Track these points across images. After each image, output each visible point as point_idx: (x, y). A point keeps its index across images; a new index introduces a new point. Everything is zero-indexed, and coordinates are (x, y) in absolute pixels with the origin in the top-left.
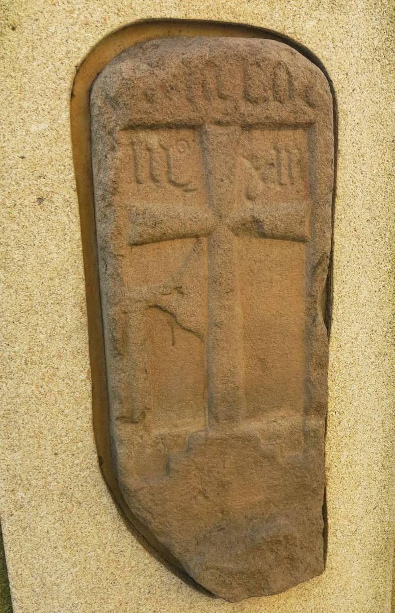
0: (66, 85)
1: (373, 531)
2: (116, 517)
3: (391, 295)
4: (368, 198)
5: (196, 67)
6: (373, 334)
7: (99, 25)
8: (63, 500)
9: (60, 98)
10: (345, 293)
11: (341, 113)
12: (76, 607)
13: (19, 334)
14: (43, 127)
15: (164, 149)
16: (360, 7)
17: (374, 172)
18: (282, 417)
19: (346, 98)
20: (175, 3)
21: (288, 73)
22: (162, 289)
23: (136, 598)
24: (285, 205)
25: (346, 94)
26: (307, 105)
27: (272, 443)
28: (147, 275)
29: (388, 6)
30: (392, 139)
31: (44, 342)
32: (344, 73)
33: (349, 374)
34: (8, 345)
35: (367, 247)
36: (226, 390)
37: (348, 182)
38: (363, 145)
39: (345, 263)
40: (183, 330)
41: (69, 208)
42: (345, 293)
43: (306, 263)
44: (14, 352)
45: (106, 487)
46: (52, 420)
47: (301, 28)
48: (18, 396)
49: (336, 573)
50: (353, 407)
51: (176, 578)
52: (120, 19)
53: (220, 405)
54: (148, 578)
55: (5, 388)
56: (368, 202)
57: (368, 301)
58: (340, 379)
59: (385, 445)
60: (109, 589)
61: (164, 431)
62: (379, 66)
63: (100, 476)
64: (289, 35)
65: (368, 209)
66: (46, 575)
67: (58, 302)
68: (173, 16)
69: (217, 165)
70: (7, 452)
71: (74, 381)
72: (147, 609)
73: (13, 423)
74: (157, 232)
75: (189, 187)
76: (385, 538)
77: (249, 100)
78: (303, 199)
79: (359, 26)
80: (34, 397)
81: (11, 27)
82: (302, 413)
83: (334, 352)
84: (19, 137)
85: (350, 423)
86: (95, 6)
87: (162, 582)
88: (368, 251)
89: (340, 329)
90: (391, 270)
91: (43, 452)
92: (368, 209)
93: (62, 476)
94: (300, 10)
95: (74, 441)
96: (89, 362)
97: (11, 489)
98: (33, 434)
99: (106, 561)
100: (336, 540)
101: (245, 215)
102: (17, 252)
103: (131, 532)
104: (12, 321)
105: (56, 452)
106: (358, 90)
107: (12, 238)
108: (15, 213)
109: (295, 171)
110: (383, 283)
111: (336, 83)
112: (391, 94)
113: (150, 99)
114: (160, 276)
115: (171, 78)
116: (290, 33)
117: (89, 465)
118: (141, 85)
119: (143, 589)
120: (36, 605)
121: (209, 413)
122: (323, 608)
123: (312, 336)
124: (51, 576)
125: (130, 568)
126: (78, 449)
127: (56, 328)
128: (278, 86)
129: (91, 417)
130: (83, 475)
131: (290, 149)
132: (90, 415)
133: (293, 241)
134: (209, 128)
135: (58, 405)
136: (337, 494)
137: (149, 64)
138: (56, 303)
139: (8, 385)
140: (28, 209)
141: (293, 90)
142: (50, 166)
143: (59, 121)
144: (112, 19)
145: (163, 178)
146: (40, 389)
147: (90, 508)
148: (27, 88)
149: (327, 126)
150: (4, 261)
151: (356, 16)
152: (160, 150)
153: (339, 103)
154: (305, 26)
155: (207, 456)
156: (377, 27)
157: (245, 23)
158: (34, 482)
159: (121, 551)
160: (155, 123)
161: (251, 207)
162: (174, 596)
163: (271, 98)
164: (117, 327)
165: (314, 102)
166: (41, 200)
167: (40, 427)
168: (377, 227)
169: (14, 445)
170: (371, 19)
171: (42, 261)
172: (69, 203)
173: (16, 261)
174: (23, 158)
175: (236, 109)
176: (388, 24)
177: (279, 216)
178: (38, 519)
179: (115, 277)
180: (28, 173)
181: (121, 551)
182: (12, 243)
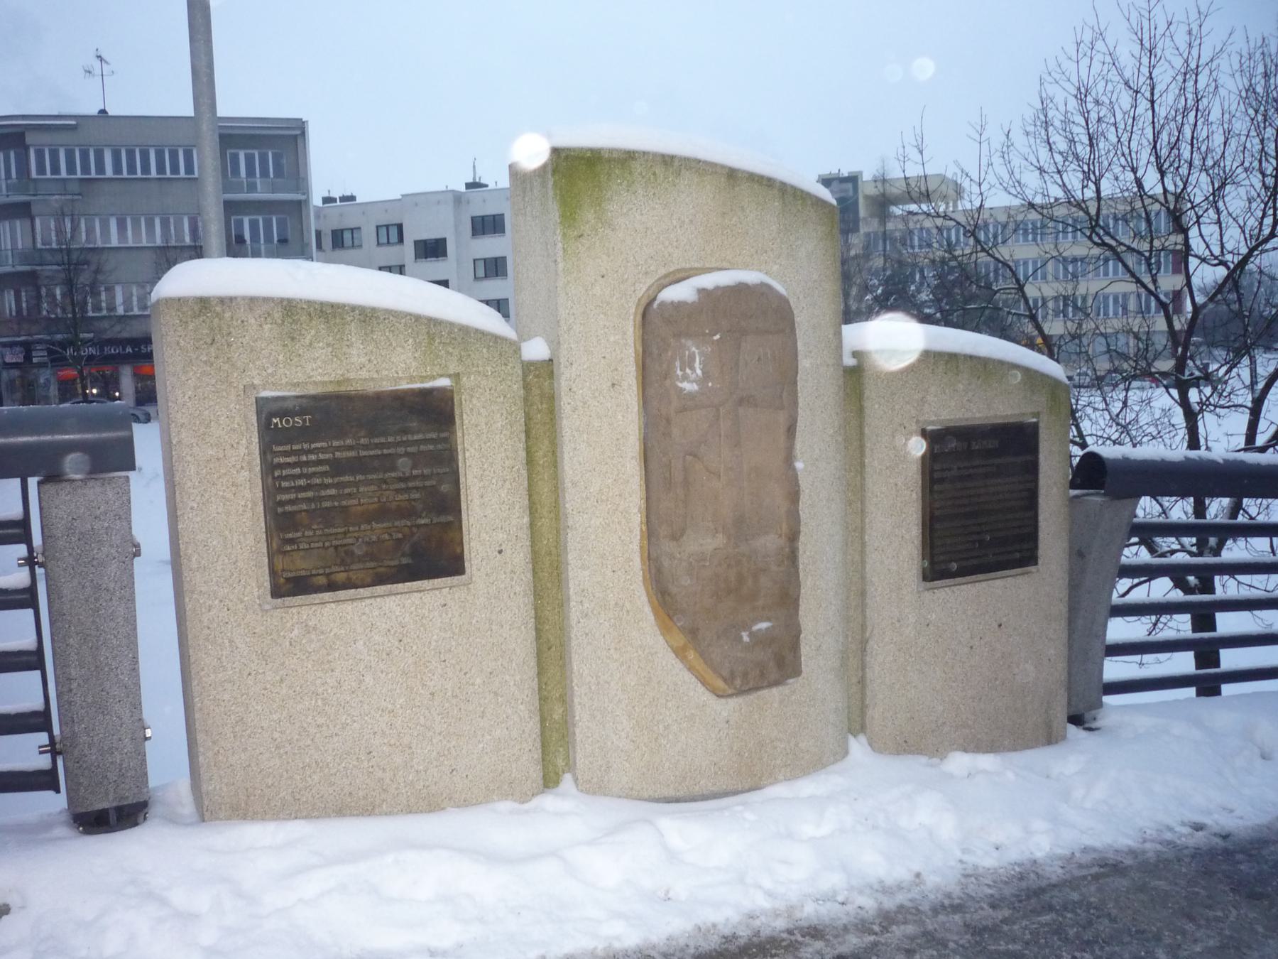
174: (604, 357)
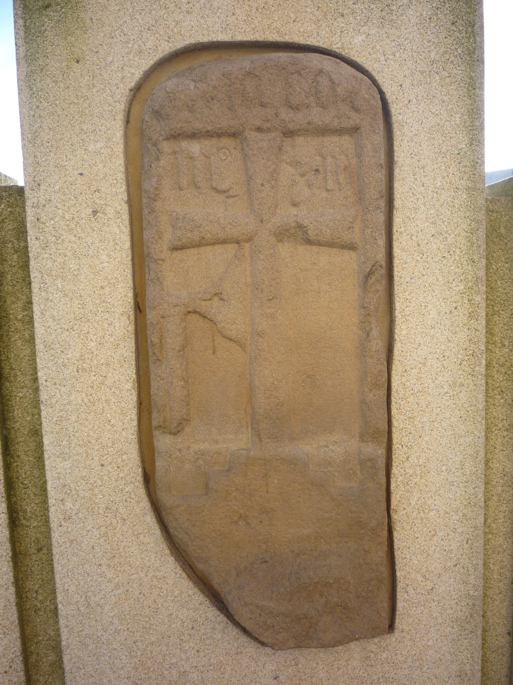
1: (454, 593)
2: (160, 538)
3: (466, 319)
4: (432, 211)
6: (445, 360)
7: (151, 51)
8: (108, 515)
9: (115, 119)
10: (409, 312)
11: (396, 124)
12: (118, 634)
13: (72, 341)
15: (206, 157)
16: (413, 21)
18: (334, 441)
19: (401, 109)
20: (222, 28)
21: (331, 80)
22: (201, 295)
24: (332, 211)
25: (401, 105)
26: (352, 110)
27: (322, 470)
29: (444, 20)
30: (457, 152)
31: (94, 350)
33: (417, 403)
34: (63, 352)
36: (269, 404)
37: (406, 194)
38: (423, 157)
40: (224, 339)
41: (120, 220)
42: (409, 312)
43: (357, 272)
44: (67, 359)
46: (100, 430)
47: (349, 43)
48: (69, 403)
49: (408, 637)
50: (424, 442)
51: (222, 616)
52: (170, 45)
53: (263, 422)
54: (191, 611)
55: (59, 395)
56: (433, 216)
57: (438, 323)
59: (465, 491)
60: (152, 619)
62: (438, 78)
63: (145, 492)
64: (337, 50)
65: (432, 223)
67: (107, 310)
68: (219, 39)
69: (257, 170)
70: (58, 460)
71: (121, 391)
72: (190, 648)
73: (64, 430)
74: (196, 236)
75: (231, 193)
76: (471, 603)
77: (291, 107)
78: (351, 205)
79: (413, 39)
80: (84, 405)
81: (75, 60)
82: (358, 439)
83: (398, 377)
84: (78, 156)
85: (420, 460)
86: (148, 35)
88: (434, 268)
89: (405, 352)
90: (464, 290)
91: (91, 463)
92: (432, 223)
93: (108, 489)
94: (348, 26)
96: (135, 371)
98: (82, 443)
99: (148, 586)
100: (407, 598)
101: (288, 220)
102: (73, 262)
103: (175, 557)
104: (66, 328)
105: (103, 463)
106: (414, 101)
107: (70, 249)
108: (73, 226)
109: (342, 178)
111: (389, 95)
112: (453, 106)
113: (191, 109)
114: (200, 282)
115: (211, 89)
116: (338, 48)
117: (133, 480)
118: (183, 97)
119: (186, 624)
120: (80, 625)
121: (251, 430)
122: (393, 678)
123: (367, 351)
124: (95, 596)
125: (173, 598)
126: (123, 461)
127: (105, 336)
128: (320, 92)
130: (127, 490)
131: (336, 155)
132: (135, 426)
133: (342, 248)
134: (249, 134)
135: (105, 415)
136: (407, 542)
139: (61, 392)
140: (84, 221)
141: (336, 95)
142: (104, 181)
143: (114, 140)
144: (163, 46)
146: (89, 396)
147: (134, 525)
150: (62, 270)
151: (408, 30)
152: (202, 157)
153: (393, 114)
154: (353, 41)
156: (433, 40)
157: (291, 41)
159: (164, 577)
160: (196, 131)
161: (295, 213)
162: (219, 636)
163: (313, 104)
164: (155, 331)
165: (359, 107)
166: (95, 212)
167: (88, 436)
169: (65, 452)
170: (426, 33)
171: (95, 270)
172: (120, 215)
173: (72, 270)
174: (81, 174)
175: (277, 116)
176: (446, 38)
177: (324, 222)
178: (85, 533)
179: (155, 281)
180: (85, 188)
181: (164, 577)
182: (69, 254)
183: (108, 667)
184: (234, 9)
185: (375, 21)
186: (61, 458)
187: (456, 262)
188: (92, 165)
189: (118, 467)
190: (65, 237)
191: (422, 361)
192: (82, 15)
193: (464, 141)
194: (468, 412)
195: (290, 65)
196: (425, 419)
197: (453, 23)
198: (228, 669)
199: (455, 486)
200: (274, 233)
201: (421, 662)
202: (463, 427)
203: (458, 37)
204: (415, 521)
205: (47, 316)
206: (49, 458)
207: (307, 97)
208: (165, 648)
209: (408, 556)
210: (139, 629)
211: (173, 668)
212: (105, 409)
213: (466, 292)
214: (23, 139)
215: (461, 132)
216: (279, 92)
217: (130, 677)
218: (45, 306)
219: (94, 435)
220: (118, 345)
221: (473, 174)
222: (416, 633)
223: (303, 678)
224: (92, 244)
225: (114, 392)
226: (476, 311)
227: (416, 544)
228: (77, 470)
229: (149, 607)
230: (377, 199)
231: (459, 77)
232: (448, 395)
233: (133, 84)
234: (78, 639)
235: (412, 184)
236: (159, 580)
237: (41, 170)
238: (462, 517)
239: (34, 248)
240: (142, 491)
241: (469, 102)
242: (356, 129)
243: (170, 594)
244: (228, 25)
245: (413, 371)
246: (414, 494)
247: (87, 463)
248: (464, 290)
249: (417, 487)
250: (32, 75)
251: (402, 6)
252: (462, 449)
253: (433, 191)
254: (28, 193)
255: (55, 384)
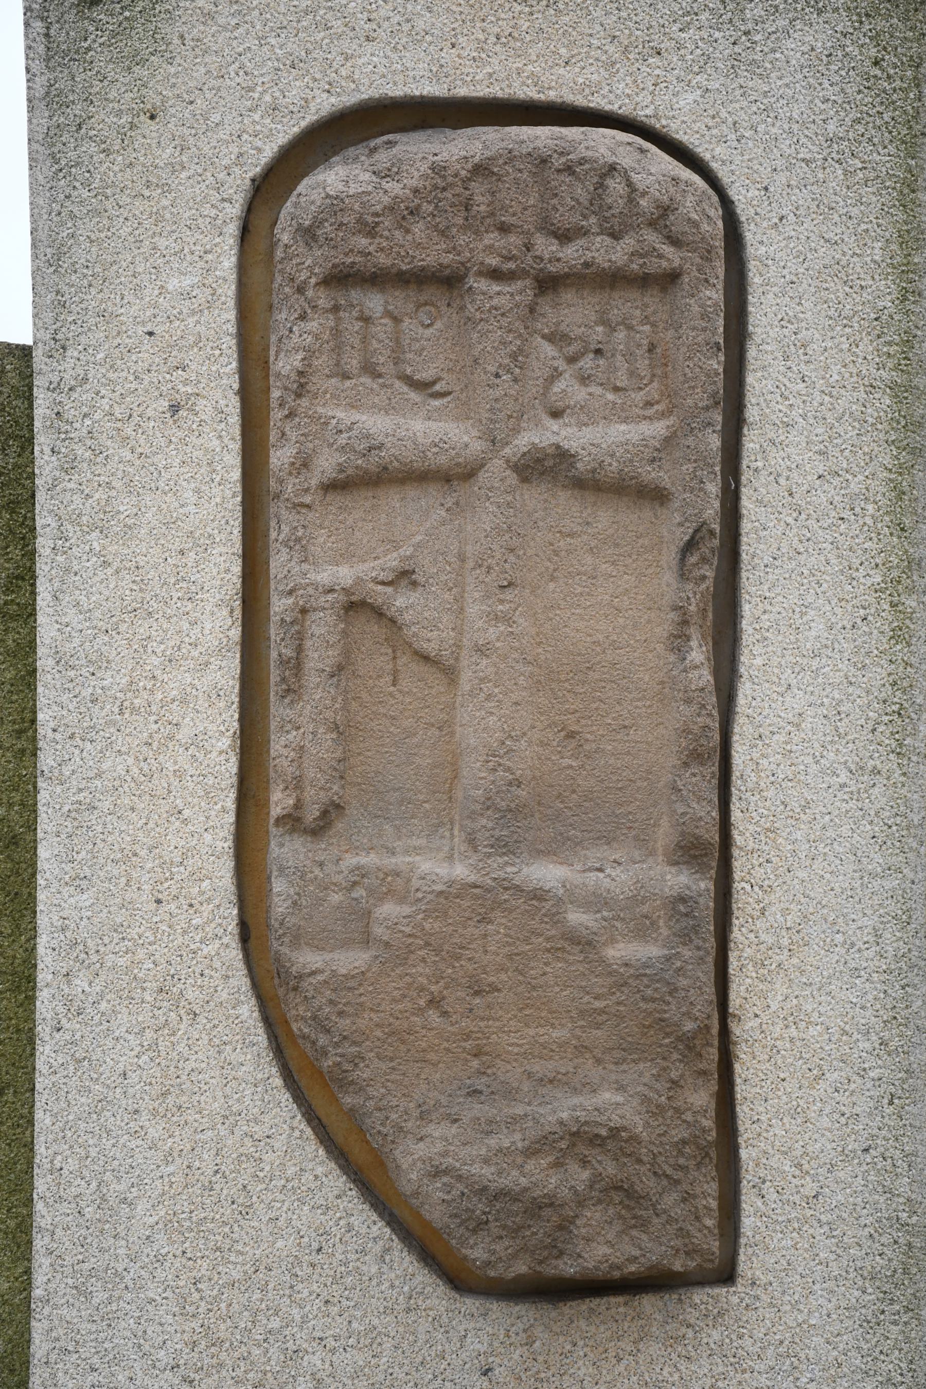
0: (234, 211)
1: (865, 1211)
5: (456, 175)
7: (295, 110)
14: (188, 282)
17: (831, 380)
18: (615, 861)
21: (630, 184)
23: (291, 1259)
28: (351, 544)
30: (873, 316)
31: (158, 673)
32: (759, 186)
35: (820, 531)
37: (769, 397)
39: (768, 560)
41: (223, 425)
45: (249, 983)
46: (158, 829)
48: (99, 775)
52: (333, 100)
54: (319, 1211)
56: (821, 438)
57: (826, 646)
58: (761, 811)
60: (236, 1229)
61: (368, 860)
62: (840, 172)
63: (241, 956)
66: (108, 1176)
68: (425, 93)
70: (65, 891)
74: (372, 463)
75: (437, 387)
80: (129, 779)
85: (789, 918)
87: (350, 1228)
89: (759, 699)
90: (883, 585)
91: (135, 896)
92: (820, 453)
93: (166, 950)
95: (196, 877)
96: (236, 716)
97: (64, 971)
100: (763, 1208)
105: (160, 896)
106: (791, 217)
107: (120, 474)
108: (129, 431)
110: (862, 612)
112: (869, 226)
119: (306, 1239)
124: (119, 1179)
125: (283, 1182)
129: (232, 828)
130: (205, 951)
131: (634, 323)
136: (762, 1087)
137: (374, 173)
138: (186, 597)
142: (196, 350)
143: (217, 273)
145: (388, 369)
148: (168, 216)
149: (707, 281)
155: (450, 921)
158: (110, 960)
163: (595, 229)
166: (175, 408)
168: (843, 492)
174: (151, 334)
175: (528, 250)
176: (859, 92)
178: (109, 1043)
182: (117, 484)
183: (130, 1345)
184: (455, 36)
185: (720, 65)
186: (73, 888)
187: (866, 528)
188: (172, 318)
189: (191, 905)
190: (111, 451)
191: (792, 719)
192: (165, 29)
193: (889, 293)
194: (890, 827)
195: (555, 156)
196: (799, 835)
197: (876, 63)
198: (388, 1344)
199: (863, 980)
200: (516, 465)
201: (796, 1363)
202: (878, 858)
203: (884, 91)
204: (778, 1043)
205: (64, 603)
206: (47, 887)
207: (585, 217)
208: (257, 1295)
209: (763, 1118)
210: (207, 1253)
211: (272, 1342)
212: (172, 788)
213: (887, 589)
214: (35, 257)
215: (883, 277)
216: (534, 206)
217: (178, 1366)
218: (63, 582)
219: (145, 840)
220: (207, 664)
221: (905, 358)
222: (784, 1293)
223: (543, 1375)
224: (165, 468)
225: (193, 756)
226: (908, 627)
227: (780, 1093)
228: (105, 911)
229: (233, 1203)
230: (707, 408)
231: (884, 169)
232: (847, 789)
233: (258, 169)
234: (70, 1281)
235: (780, 378)
236: (257, 1143)
237: (70, 319)
238: (877, 1046)
239: (48, 469)
240: (235, 954)
241: (901, 216)
242: (671, 278)
243: (278, 1173)
244: (442, 66)
245: (776, 737)
246: (778, 986)
247: (128, 896)
248: (883, 585)
249: (781, 972)
250: (59, 133)
251: (774, 32)
252: (876, 902)
253: (823, 392)
254: (39, 360)
255: (72, 737)
